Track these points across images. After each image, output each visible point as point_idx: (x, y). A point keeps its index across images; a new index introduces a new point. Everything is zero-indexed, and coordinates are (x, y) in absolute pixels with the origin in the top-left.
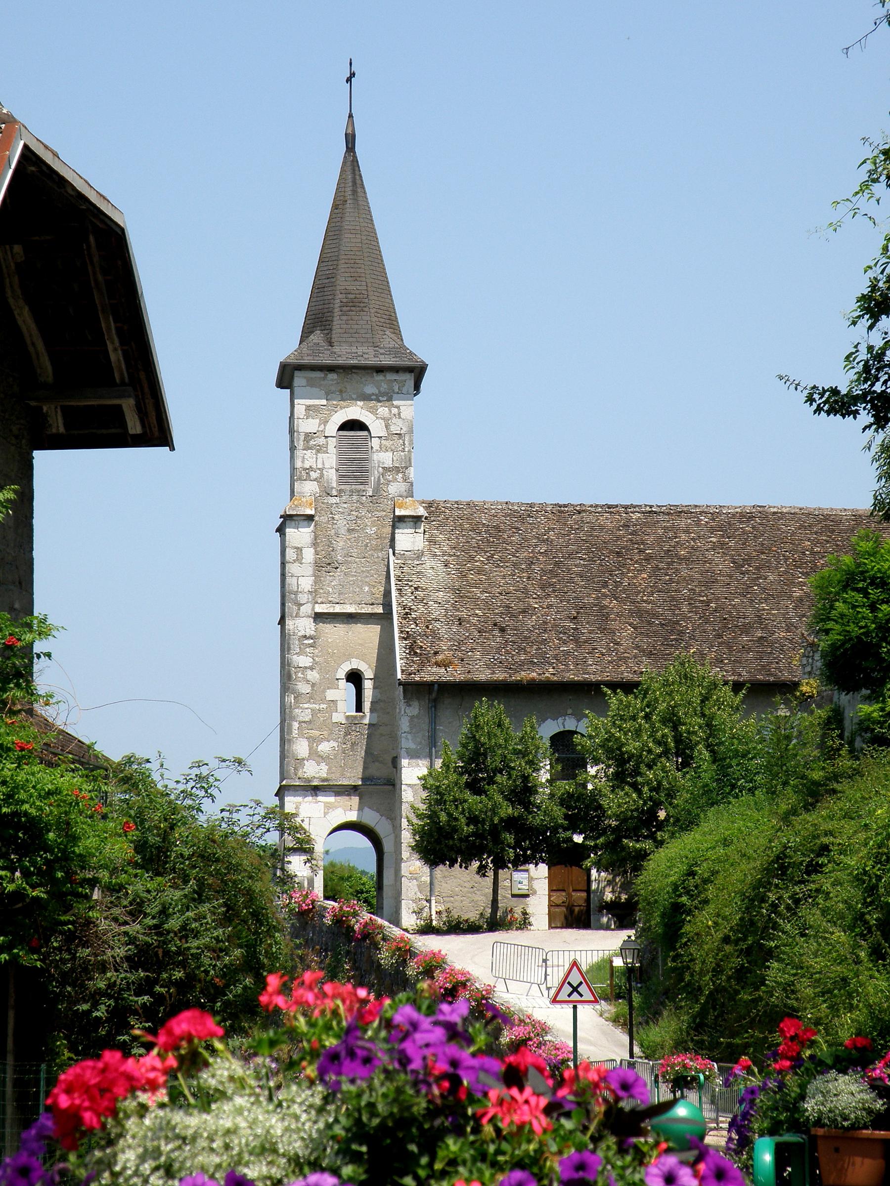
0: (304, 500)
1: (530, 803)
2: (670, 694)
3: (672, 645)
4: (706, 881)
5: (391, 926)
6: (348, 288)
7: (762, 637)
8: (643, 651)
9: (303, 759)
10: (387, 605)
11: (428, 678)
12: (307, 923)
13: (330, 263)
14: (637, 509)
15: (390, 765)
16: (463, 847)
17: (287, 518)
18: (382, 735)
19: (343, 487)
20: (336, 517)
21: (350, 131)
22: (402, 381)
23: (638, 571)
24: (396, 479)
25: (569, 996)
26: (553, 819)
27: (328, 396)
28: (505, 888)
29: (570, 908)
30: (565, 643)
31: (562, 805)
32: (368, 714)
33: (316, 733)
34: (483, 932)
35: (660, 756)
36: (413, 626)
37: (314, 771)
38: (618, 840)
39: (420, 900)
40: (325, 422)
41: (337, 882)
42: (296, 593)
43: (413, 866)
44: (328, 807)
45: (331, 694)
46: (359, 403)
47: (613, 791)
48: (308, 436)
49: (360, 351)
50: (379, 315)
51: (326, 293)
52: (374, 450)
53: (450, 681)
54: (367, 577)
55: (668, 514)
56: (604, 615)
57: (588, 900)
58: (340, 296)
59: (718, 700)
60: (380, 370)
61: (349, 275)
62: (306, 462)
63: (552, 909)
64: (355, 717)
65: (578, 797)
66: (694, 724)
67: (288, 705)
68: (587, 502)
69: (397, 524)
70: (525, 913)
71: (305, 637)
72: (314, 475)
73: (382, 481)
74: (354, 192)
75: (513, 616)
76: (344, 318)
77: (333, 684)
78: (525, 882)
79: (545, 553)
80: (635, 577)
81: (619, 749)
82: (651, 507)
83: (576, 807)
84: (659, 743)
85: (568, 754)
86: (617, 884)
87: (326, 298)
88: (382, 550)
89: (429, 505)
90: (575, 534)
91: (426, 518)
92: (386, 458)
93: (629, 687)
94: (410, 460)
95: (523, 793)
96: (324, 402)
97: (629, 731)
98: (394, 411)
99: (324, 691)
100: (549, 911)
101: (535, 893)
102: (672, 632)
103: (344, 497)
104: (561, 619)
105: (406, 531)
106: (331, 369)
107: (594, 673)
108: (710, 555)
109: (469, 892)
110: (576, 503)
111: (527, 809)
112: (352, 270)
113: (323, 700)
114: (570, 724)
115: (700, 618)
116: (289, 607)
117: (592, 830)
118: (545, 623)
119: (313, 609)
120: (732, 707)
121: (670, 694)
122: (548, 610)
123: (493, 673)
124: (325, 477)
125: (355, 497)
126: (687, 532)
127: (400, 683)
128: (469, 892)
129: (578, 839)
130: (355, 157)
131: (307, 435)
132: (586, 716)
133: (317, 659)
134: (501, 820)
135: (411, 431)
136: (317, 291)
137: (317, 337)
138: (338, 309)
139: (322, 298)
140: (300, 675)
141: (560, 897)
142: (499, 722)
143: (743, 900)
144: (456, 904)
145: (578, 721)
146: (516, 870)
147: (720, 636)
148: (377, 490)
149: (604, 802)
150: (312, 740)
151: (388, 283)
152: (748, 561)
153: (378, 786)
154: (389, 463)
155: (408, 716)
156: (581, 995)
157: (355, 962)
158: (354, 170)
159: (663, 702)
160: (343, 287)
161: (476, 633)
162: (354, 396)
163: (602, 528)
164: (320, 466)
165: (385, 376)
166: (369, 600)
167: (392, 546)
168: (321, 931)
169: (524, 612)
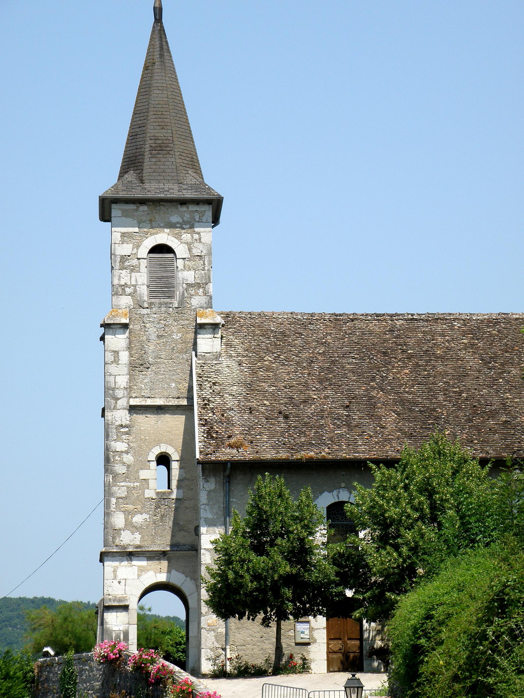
0: (120, 311)
1: (307, 562)
2: (425, 467)
3: (430, 428)
4: (441, 623)
5: (182, 671)
6: (156, 135)
7: (506, 422)
8: (405, 433)
9: (120, 530)
10: (190, 398)
11: (222, 457)
12: (115, 670)
13: (142, 115)
14: (401, 317)
16: (248, 601)
17: (106, 326)
18: (187, 508)
23: (401, 367)
24: (198, 293)
26: (326, 576)
28: (289, 637)
29: (346, 654)
30: (339, 427)
31: (334, 564)
33: (131, 507)
34: (268, 676)
35: (417, 520)
36: (210, 415)
37: (129, 539)
38: (382, 594)
39: (217, 648)
40: (138, 247)
41: (151, 633)
42: (113, 389)
43: (209, 619)
44: (142, 570)
45: (143, 474)
47: (377, 551)
48: (124, 258)
50: (183, 158)
51: (138, 140)
52: (179, 269)
53: (240, 460)
54: (173, 375)
55: (427, 321)
56: (371, 403)
57: (361, 647)
58: (150, 142)
59: (467, 472)
60: (183, 202)
61: (157, 124)
62: (122, 279)
63: (331, 656)
65: (348, 557)
66: (445, 492)
68: (360, 311)
69: (199, 331)
70: (304, 659)
71: (122, 426)
72: (128, 290)
73: (186, 295)
74: (162, 56)
75: (295, 405)
76: (154, 160)
78: (307, 632)
80: (399, 373)
81: (382, 515)
82: (412, 315)
83: (346, 566)
84: (416, 509)
85: (340, 519)
87: (138, 143)
88: (186, 352)
89: (227, 316)
90: (349, 338)
91: (223, 326)
92: (189, 276)
93: (390, 463)
94: (209, 277)
95: (301, 553)
96: (136, 230)
97: (391, 499)
98: (196, 236)
99: (137, 472)
100: (328, 657)
103: (154, 309)
104: (335, 408)
106: (142, 202)
107: (364, 452)
108: (462, 354)
109: (258, 641)
110: (349, 313)
111: (304, 567)
112: (160, 120)
113: (137, 479)
114: (343, 496)
115: (453, 406)
116: (108, 401)
117: (361, 585)
118: (322, 411)
119: (128, 402)
120: (479, 479)
121: (425, 467)
122: (325, 400)
123: (278, 452)
125: (163, 309)
126: (443, 335)
127: (199, 462)
129: (349, 593)
130: (162, 26)
132: (355, 488)
134: (280, 576)
135: (210, 253)
136: (131, 138)
137: (131, 176)
138: (148, 153)
139: (135, 144)
140: (117, 458)
141: (337, 645)
142: (280, 493)
143: (470, 639)
144: (248, 652)
146: (298, 622)
147: (470, 420)
148: (182, 302)
149: (369, 560)
150: (128, 514)
151: (191, 131)
152: (494, 358)
153: (182, 551)
154: (191, 280)
155: (207, 488)
158: (161, 37)
159: (419, 474)
160: (153, 134)
161: (264, 420)
163: (371, 333)
164: (133, 283)
165: (188, 208)
166: (175, 394)
169: (305, 402)
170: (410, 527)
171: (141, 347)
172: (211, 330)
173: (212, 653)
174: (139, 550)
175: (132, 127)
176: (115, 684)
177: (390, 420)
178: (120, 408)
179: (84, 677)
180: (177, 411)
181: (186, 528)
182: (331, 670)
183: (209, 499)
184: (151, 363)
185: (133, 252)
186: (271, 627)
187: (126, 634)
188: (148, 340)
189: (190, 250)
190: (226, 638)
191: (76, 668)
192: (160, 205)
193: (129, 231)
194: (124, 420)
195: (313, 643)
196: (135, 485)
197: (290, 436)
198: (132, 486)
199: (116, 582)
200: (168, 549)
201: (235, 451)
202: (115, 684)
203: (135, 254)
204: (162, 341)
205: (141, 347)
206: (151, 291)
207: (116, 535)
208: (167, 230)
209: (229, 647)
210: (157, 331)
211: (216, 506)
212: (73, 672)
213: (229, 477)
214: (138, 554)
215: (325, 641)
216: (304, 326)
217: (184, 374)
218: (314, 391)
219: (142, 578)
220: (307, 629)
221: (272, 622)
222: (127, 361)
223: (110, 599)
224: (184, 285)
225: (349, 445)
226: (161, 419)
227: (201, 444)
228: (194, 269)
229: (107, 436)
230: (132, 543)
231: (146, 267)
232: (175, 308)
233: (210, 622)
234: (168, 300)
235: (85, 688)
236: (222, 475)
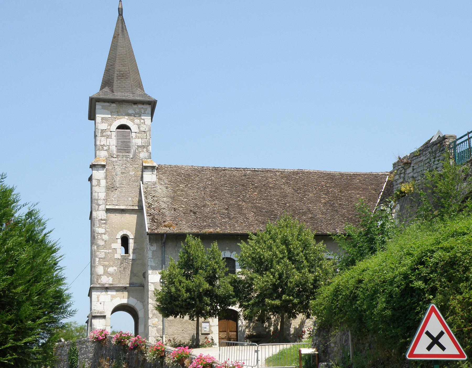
0: (101, 159)
8: (260, 222)
15: (142, 277)
19: (119, 154)
20: (116, 167)
21: (120, 7)
25: (429, 348)
27: (112, 113)
30: (224, 218)
32: (131, 255)
33: (107, 263)
37: (106, 280)
39: (158, 337)
40: (111, 125)
42: (97, 200)
44: (113, 297)
45: (114, 246)
46: (126, 117)
48: (103, 131)
49: (126, 95)
55: (262, 171)
56: (240, 209)
60: (135, 103)
64: (125, 256)
67: (93, 250)
68: (227, 166)
69: (144, 170)
72: (105, 148)
73: (137, 151)
76: (119, 81)
77: (115, 241)
78: (208, 328)
79: (211, 185)
80: (252, 194)
86: (251, 328)
88: (137, 182)
92: (139, 142)
96: (110, 116)
98: (142, 121)
99: (110, 244)
101: (212, 332)
102: (271, 214)
103: (119, 158)
106: (113, 101)
107: (239, 230)
108: (283, 186)
109: (181, 333)
113: (110, 248)
116: (94, 206)
125: (124, 158)
126: (271, 178)
127: (148, 234)
128: (181, 333)
130: (122, 17)
131: (102, 130)
137: (107, 89)
140: (99, 237)
141: (224, 335)
145: (231, 253)
148: (135, 155)
150: (105, 266)
152: (300, 189)
153: (137, 286)
154: (140, 144)
155: (151, 250)
156: (443, 348)
157: (128, 363)
162: (124, 114)
163: (234, 176)
164: (108, 144)
168: (110, 349)
170: (278, 262)
175: (107, 66)
176: (102, 355)
177: (251, 215)
179: (83, 352)
183: (153, 255)
188: (116, 175)
189: (139, 128)
191: (78, 347)
194: (103, 217)
197: (197, 222)
199: (99, 303)
200: (128, 285)
201: (168, 229)
202: (102, 355)
206: (118, 149)
208: (126, 117)
211: (157, 259)
212: (76, 349)
213: (164, 243)
215: (218, 332)
223: (95, 312)
233: (154, 322)
234: (127, 154)
235: (83, 358)
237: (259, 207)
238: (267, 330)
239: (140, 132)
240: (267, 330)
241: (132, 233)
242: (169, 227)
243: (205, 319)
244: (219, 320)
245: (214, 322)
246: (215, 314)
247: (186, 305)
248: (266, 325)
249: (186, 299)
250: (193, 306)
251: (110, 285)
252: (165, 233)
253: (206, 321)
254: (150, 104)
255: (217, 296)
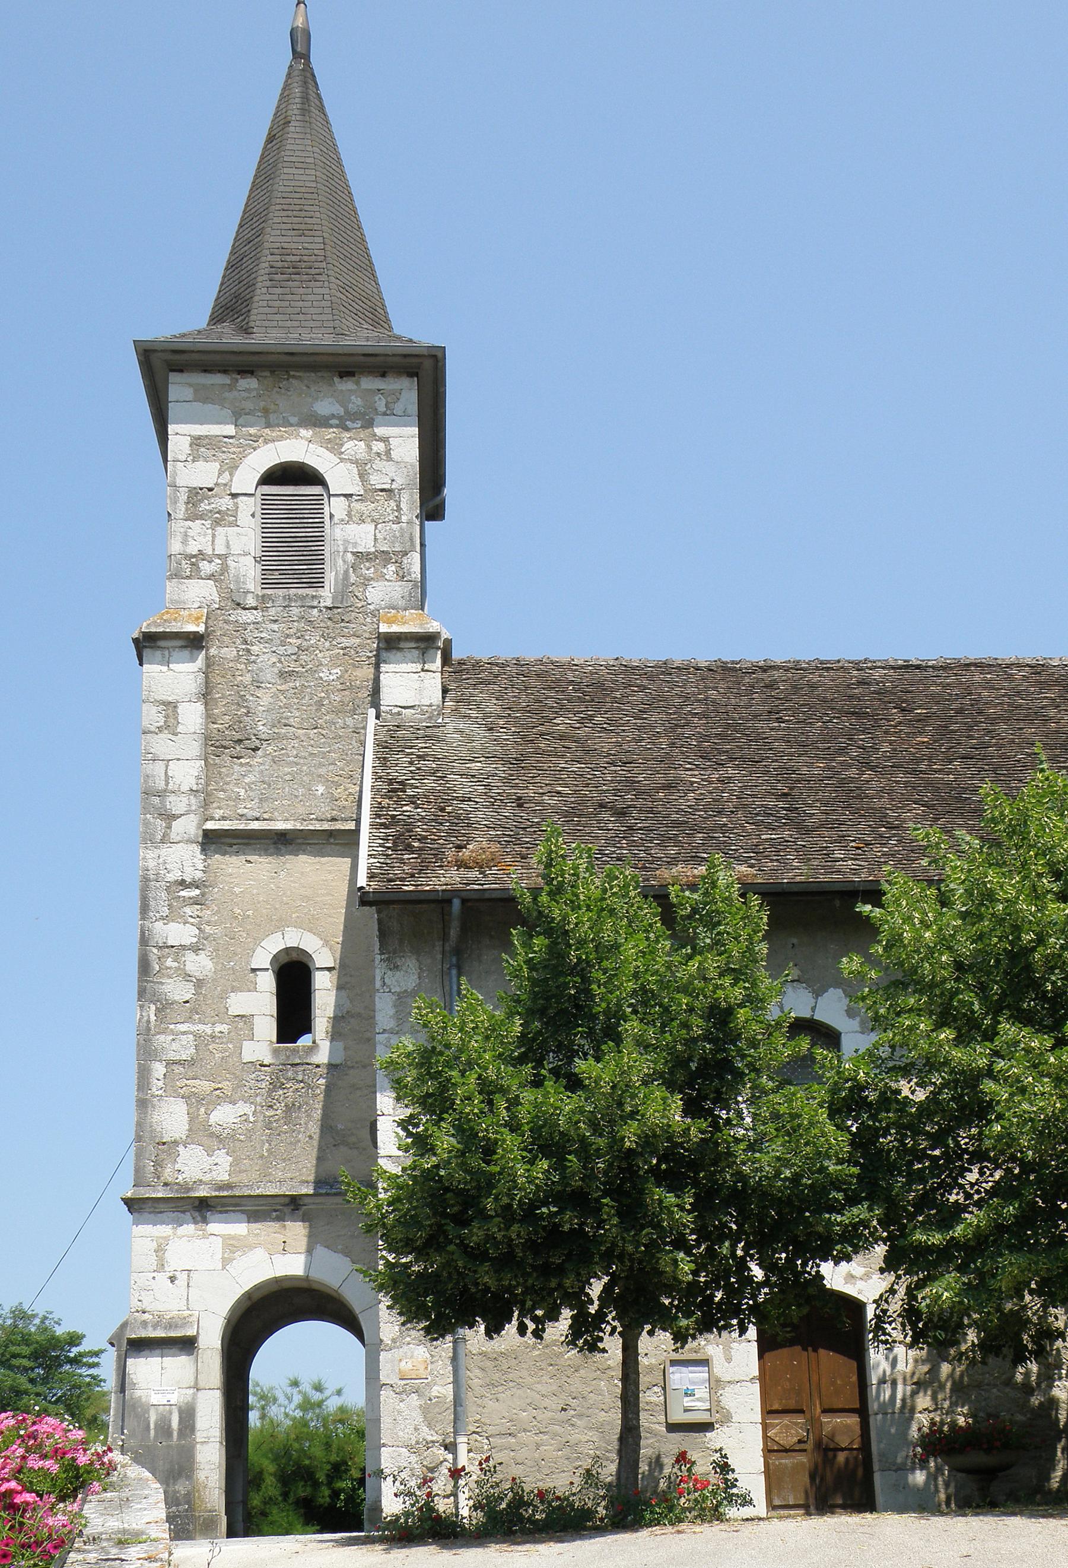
6: (285, 245)
9: (176, 1143)
20: (255, 649)
22: (393, 393)
24: (383, 575)
27: (238, 417)
29: (826, 1450)
37: (199, 1168)
39: (429, 1445)
40: (233, 468)
44: (233, 1247)
45: (238, 1003)
48: (196, 495)
54: (321, 765)
62: (191, 542)
63: (774, 1459)
68: (778, 658)
69: (384, 655)
71: (182, 884)
72: (206, 568)
73: (353, 578)
78: (702, 1392)
86: (942, 1387)
92: (363, 537)
96: (230, 429)
99: (223, 997)
100: (766, 1464)
101: (727, 1418)
103: (272, 612)
105: (404, 667)
107: (854, 871)
108: (1052, 712)
109: (553, 1422)
113: (222, 1014)
124: (232, 571)
125: (295, 611)
133: (208, 929)
140: (169, 962)
144: (522, 1454)
145: (817, 994)
148: (344, 590)
150: (195, 1101)
154: (366, 544)
164: (220, 550)
165: (358, 383)
167: (375, 703)
171: (236, 699)
172: (416, 653)
173: (414, 1458)
174: (225, 1193)
178: (179, 838)
180: (329, 848)
181: (353, 1139)
182: (777, 1502)
184: (263, 737)
185: (220, 481)
186: (604, 1351)
187: (188, 1415)
188: (257, 684)
189: (363, 476)
190: (455, 1413)
192: (289, 377)
193: (211, 433)
195: (722, 1423)
196: (217, 1030)
198: (209, 1032)
199: (163, 1278)
200: (309, 1190)
203: (225, 485)
204: (291, 684)
205: (236, 699)
207: (163, 1156)
208: (305, 433)
209: (464, 1439)
210: (280, 662)
213: (458, 952)
214: (223, 1206)
215: (758, 1418)
216: (651, 678)
217: (348, 763)
218: (691, 770)
219: (234, 1268)
220: (703, 1383)
221: (606, 1338)
222: (198, 727)
223: (145, 1324)
224: (349, 555)
225: (809, 860)
226: (288, 866)
227: (372, 860)
228: (373, 521)
229: (145, 909)
230: (207, 1178)
231: (253, 515)
232: (327, 608)
233: (406, 1366)
234: (311, 592)
236: (438, 949)
237: (948, 784)
238: (1035, 1400)
239: (370, 493)
240: (1035, 1400)
241: (326, 943)
242: (480, 866)
243: (681, 1338)
244: (765, 1346)
245: (735, 1358)
246: (736, 1312)
247: (531, 1245)
248: (1027, 1374)
249: (533, 1205)
250: (583, 1254)
251: (220, 1188)
252: (456, 892)
253: (686, 1354)
254: (411, 374)
255: (742, 1195)
